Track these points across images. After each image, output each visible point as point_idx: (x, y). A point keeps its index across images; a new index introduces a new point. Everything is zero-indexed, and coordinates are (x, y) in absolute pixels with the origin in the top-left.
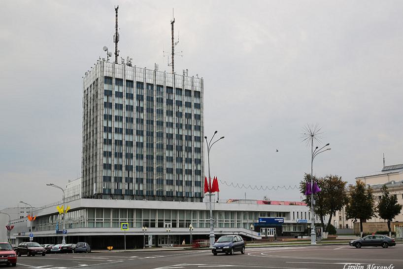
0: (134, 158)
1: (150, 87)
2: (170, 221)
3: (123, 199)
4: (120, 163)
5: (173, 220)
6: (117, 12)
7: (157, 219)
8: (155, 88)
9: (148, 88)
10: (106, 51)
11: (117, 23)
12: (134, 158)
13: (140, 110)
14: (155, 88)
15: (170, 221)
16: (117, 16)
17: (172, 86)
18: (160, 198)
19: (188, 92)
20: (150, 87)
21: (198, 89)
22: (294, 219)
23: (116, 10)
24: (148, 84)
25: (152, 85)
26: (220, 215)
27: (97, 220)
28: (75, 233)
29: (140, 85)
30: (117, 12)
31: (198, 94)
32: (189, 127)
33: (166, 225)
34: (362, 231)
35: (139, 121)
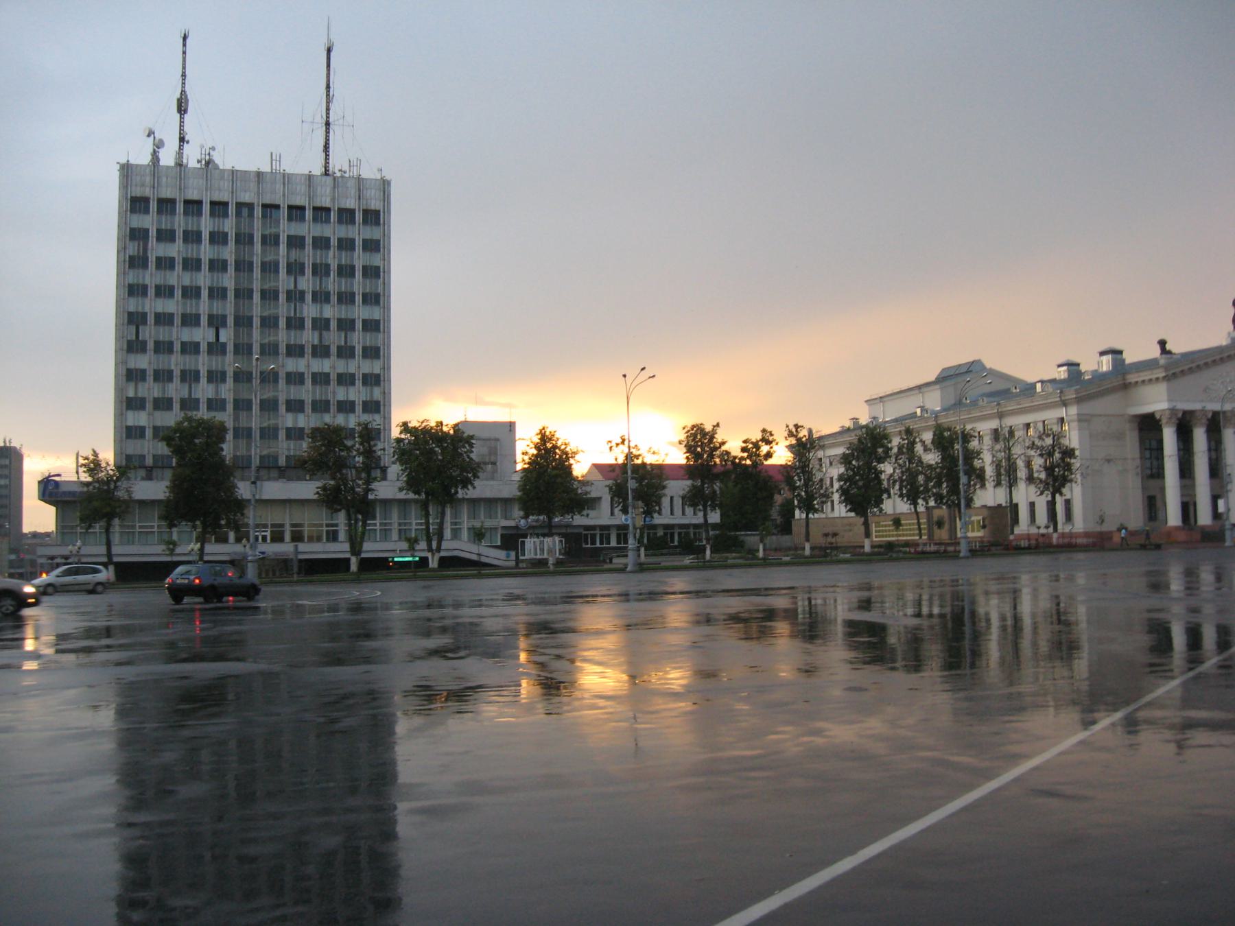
0: (203, 380)
1: (245, 211)
2: (265, 526)
3: (151, 479)
4: (352, 397)
5: (273, 526)
6: (184, 45)
7: (287, 522)
8: (258, 212)
9: (238, 214)
10: (149, 136)
11: (184, 68)
12: (203, 380)
13: (218, 266)
14: (258, 212)
15: (265, 526)
16: (184, 53)
17: (328, 205)
18: (274, 473)
19: (346, 216)
20: (245, 211)
21: (375, 205)
22: (672, 513)
23: (185, 38)
24: (240, 205)
25: (250, 206)
26: (404, 514)
27: (141, 527)
28: (143, 555)
29: (219, 207)
30: (184, 45)
31: (374, 217)
32: (346, 298)
33: (257, 538)
34: (868, 534)
35: (217, 293)
